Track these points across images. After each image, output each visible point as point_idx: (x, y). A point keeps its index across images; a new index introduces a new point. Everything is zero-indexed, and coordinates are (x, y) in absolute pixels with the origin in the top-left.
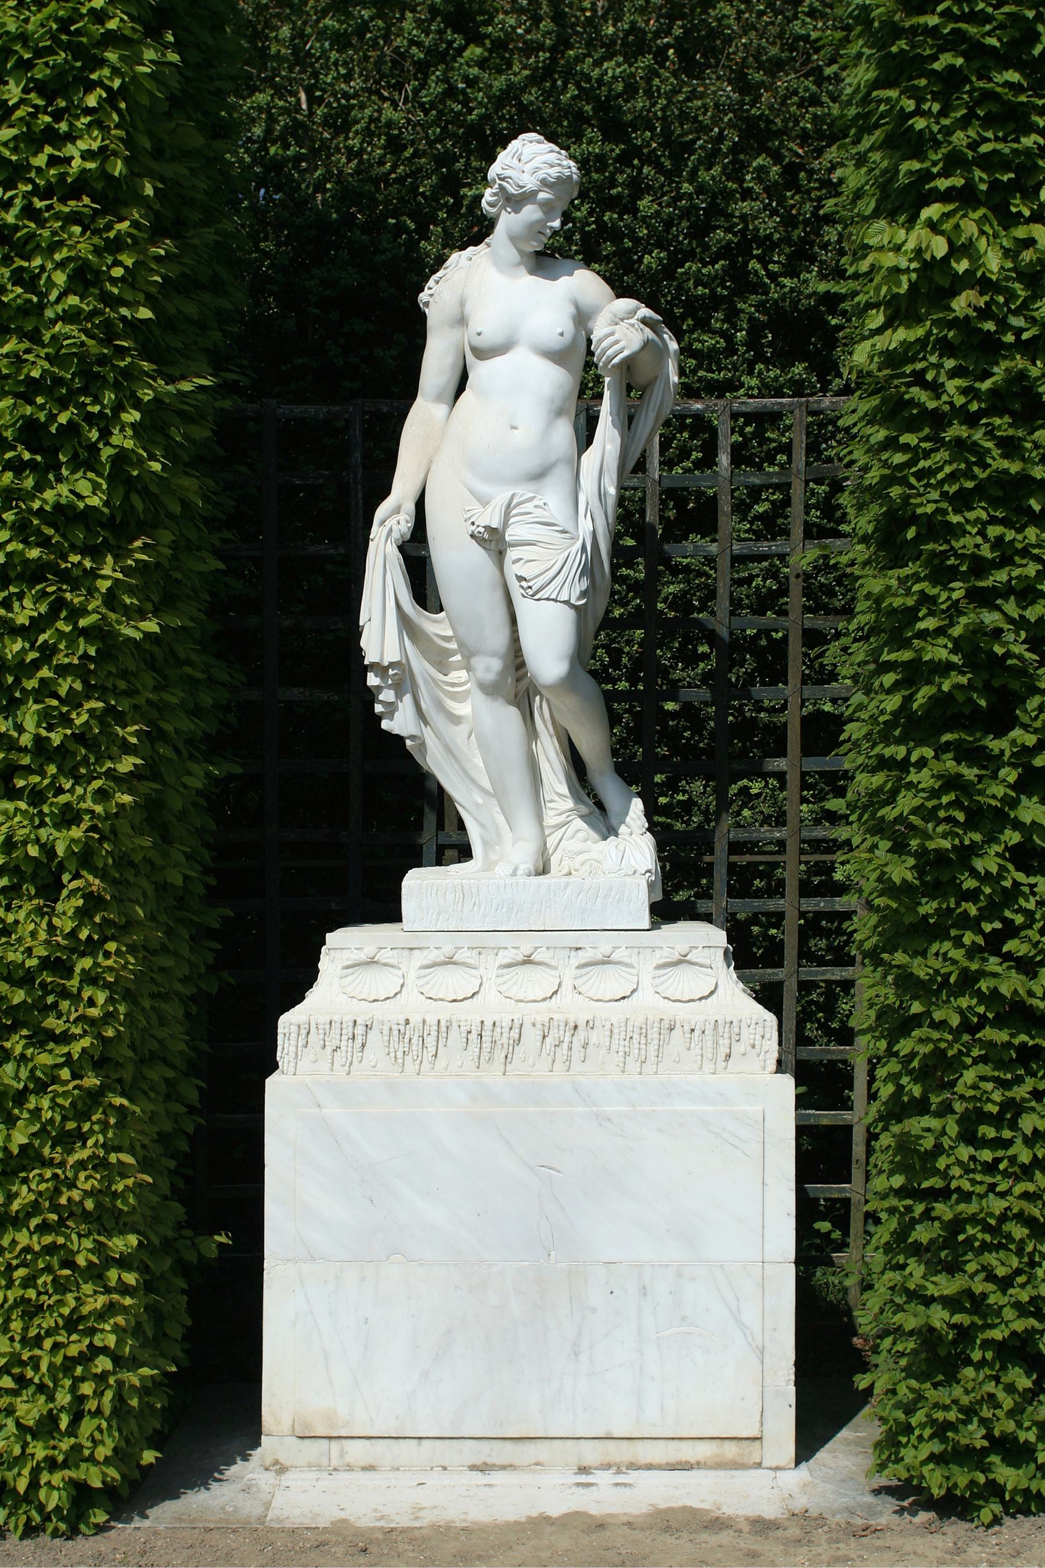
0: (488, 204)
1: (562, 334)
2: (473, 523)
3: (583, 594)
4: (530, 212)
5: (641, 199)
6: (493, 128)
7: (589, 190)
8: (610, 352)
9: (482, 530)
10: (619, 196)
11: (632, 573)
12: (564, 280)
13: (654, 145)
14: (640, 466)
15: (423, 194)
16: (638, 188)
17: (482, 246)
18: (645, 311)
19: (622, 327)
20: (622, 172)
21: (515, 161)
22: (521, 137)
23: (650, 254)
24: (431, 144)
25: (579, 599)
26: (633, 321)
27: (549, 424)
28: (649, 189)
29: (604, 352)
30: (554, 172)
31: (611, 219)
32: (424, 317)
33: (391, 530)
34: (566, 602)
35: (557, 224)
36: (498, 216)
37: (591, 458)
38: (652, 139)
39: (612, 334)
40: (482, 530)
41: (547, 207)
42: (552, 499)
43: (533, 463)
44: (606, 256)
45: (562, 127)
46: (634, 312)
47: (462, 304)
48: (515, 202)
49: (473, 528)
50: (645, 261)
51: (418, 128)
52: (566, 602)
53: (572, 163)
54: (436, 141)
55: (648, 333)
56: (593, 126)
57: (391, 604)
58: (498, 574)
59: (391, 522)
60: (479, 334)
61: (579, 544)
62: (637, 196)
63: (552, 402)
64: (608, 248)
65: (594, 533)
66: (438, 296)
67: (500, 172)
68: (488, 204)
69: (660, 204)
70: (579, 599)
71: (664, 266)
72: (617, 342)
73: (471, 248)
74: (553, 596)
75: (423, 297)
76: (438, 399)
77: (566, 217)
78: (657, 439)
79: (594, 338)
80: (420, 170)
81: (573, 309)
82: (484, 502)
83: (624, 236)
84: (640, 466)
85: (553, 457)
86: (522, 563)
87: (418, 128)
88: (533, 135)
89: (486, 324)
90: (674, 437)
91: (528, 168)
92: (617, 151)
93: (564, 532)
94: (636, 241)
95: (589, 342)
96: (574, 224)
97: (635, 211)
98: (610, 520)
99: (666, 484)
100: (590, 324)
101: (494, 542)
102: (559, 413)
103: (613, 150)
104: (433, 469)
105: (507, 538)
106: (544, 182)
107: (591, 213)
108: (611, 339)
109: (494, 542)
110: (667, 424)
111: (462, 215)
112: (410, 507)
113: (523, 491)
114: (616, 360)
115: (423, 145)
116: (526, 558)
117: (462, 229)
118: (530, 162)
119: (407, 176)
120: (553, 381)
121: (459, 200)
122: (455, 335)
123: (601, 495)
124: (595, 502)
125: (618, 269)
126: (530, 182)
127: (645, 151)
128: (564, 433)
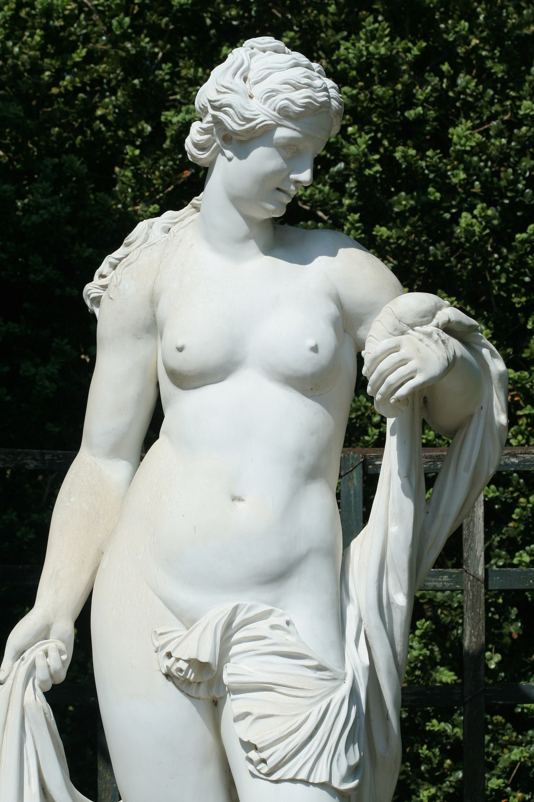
0: (196, 145)
1: (315, 349)
2: (169, 655)
3: (353, 771)
4: (263, 159)
5: (455, 126)
6: (216, 16)
7: (370, 111)
8: (392, 378)
9: (184, 666)
10: (421, 120)
11: (448, 728)
12: (321, 262)
13: (475, 42)
14: (453, 552)
15: (103, 118)
16: (448, 109)
17: (187, 210)
18: (449, 312)
19: (413, 337)
20: (424, 83)
21: (238, 80)
22: (249, 43)
23: (470, 210)
24: (115, 41)
25: (345, 780)
26: (430, 328)
27: (295, 495)
28: (468, 109)
29: (383, 378)
30: (300, 97)
31: (405, 156)
32: (92, 319)
33: (33, 666)
34: (325, 786)
35: (306, 176)
36: (213, 163)
37: (365, 546)
38: (471, 31)
39: (396, 349)
40: (184, 666)
41: (289, 150)
42: (302, 612)
43: (269, 555)
44: (400, 214)
45: (326, 13)
46: (432, 313)
47: (153, 302)
48: (241, 142)
49: (169, 662)
50: (463, 222)
51: (95, 17)
52: (325, 786)
53: (330, 83)
54: (125, 37)
55: (455, 346)
56: (375, 13)
57: (220, 617)
58: (210, 738)
59: (35, 653)
60: (180, 349)
61: (345, 689)
62: (448, 120)
63: (300, 456)
64: (403, 201)
65: (372, 670)
66: (117, 288)
67: (214, 96)
68: (196, 145)
69: (486, 133)
70: (345, 780)
71: (493, 229)
72: (403, 362)
73: (169, 214)
74: (302, 776)
75: (91, 290)
76: (114, 452)
77: (321, 166)
78: (480, 511)
79: (367, 355)
80: (98, 81)
81: (332, 309)
82: (188, 621)
83: (428, 182)
84: (453, 552)
85: (302, 547)
86: (249, 720)
87: (95, 17)
88: (268, 41)
89: (191, 335)
90: (515, 503)
91: (258, 90)
92: (415, 51)
93: (320, 668)
94: (448, 190)
95: (360, 361)
96: (347, 164)
97: (442, 143)
98: (399, 648)
99: (496, 584)
100: (361, 332)
101: (204, 685)
102: (312, 474)
103: (408, 50)
104: (104, 565)
105: (226, 679)
106: (285, 113)
107: (374, 146)
108: (394, 358)
109: (204, 685)
110: (500, 479)
111: (166, 152)
112: (65, 628)
113: (253, 602)
114: (403, 391)
115: (102, 43)
116: (257, 711)
117: (165, 174)
118: (262, 81)
119: (77, 90)
120: (302, 423)
121: (160, 129)
122: (142, 349)
123: (383, 607)
124: (372, 621)
125: (419, 234)
126: (262, 112)
127: (461, 50)
128: (319, 506)
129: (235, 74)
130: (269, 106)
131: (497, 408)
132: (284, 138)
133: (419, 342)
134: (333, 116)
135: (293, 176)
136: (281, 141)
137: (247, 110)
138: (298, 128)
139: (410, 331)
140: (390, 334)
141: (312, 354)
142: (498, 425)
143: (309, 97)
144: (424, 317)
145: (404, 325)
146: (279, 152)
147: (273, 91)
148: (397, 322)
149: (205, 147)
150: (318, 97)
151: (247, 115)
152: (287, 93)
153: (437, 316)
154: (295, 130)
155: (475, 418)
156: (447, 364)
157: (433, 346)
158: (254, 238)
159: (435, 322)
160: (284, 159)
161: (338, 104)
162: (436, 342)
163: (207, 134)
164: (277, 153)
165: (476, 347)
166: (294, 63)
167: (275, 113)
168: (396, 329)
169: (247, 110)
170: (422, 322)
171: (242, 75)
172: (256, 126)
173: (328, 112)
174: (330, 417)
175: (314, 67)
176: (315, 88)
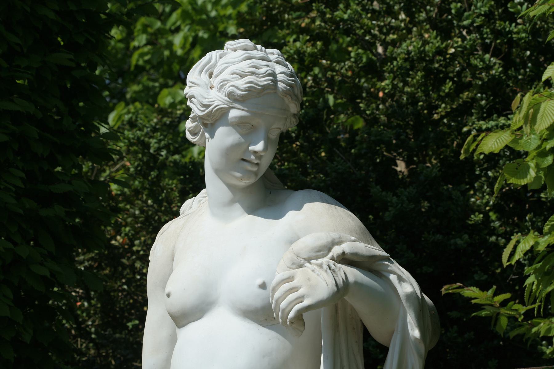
12: (292, 217)
26: (326, 260)
39: (290, 279)
72: (294, 290)
129: (201, 71)
130: (222, 94)
131: (411, 324)
132: (236, 117)
133: (312, 273)
134: (282, 96)
135: (251, 148)
136: (233, 120)
137: (205, 98)
138: (245, 109)
139: (307, 264)
140: (289, 267)
141: (261, 291)
142: (413, 339)
143: (251, 82)
144: (319, 251)
145: (301, 259)
146: (236, 129)
147: (224, 81)
148: (295, 258)
149: (196, 132)
150: (260, 82)
151: (205, 102)
152: (234, 81)
153: (333, 250)
154: (243, 110)
155: (395, 333)
156: (336, 289)
157: (324, 274)
158: (238, 201)
159: (331, 255)
160: (241, 134)
161: (285, 86)
162: (326, 271)
163: (195, 122)
164: (234, 130)
165: (385, 274)
166: (246, 57)
167: (226, 98)
168: (293, 264)
169: (205, 98)
170: (317, 256)
171: (206, 71)
172: (212, 111)
173: (276, 93)
174: (287, 343)
175: (271, 59)
176: (259, 74)
